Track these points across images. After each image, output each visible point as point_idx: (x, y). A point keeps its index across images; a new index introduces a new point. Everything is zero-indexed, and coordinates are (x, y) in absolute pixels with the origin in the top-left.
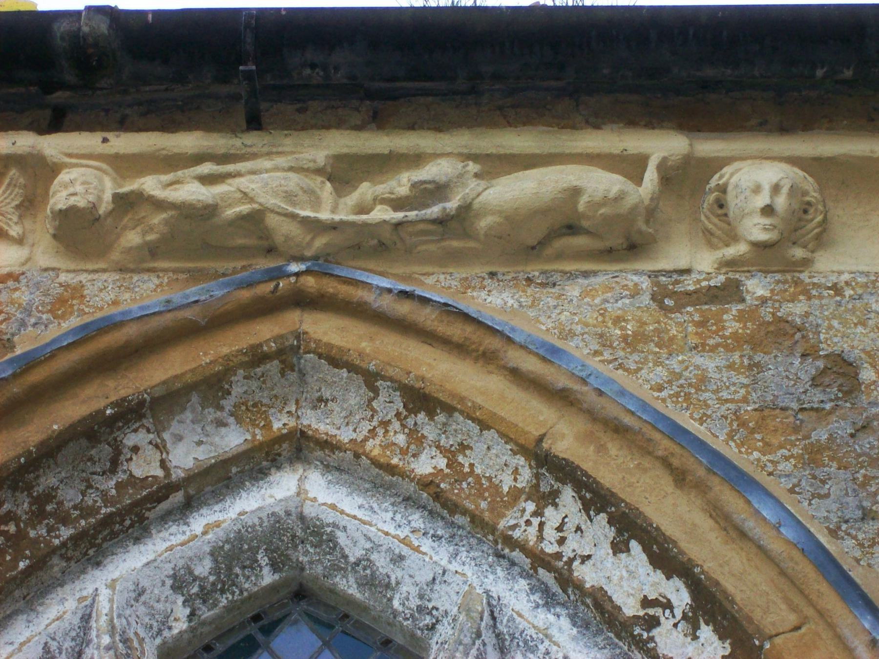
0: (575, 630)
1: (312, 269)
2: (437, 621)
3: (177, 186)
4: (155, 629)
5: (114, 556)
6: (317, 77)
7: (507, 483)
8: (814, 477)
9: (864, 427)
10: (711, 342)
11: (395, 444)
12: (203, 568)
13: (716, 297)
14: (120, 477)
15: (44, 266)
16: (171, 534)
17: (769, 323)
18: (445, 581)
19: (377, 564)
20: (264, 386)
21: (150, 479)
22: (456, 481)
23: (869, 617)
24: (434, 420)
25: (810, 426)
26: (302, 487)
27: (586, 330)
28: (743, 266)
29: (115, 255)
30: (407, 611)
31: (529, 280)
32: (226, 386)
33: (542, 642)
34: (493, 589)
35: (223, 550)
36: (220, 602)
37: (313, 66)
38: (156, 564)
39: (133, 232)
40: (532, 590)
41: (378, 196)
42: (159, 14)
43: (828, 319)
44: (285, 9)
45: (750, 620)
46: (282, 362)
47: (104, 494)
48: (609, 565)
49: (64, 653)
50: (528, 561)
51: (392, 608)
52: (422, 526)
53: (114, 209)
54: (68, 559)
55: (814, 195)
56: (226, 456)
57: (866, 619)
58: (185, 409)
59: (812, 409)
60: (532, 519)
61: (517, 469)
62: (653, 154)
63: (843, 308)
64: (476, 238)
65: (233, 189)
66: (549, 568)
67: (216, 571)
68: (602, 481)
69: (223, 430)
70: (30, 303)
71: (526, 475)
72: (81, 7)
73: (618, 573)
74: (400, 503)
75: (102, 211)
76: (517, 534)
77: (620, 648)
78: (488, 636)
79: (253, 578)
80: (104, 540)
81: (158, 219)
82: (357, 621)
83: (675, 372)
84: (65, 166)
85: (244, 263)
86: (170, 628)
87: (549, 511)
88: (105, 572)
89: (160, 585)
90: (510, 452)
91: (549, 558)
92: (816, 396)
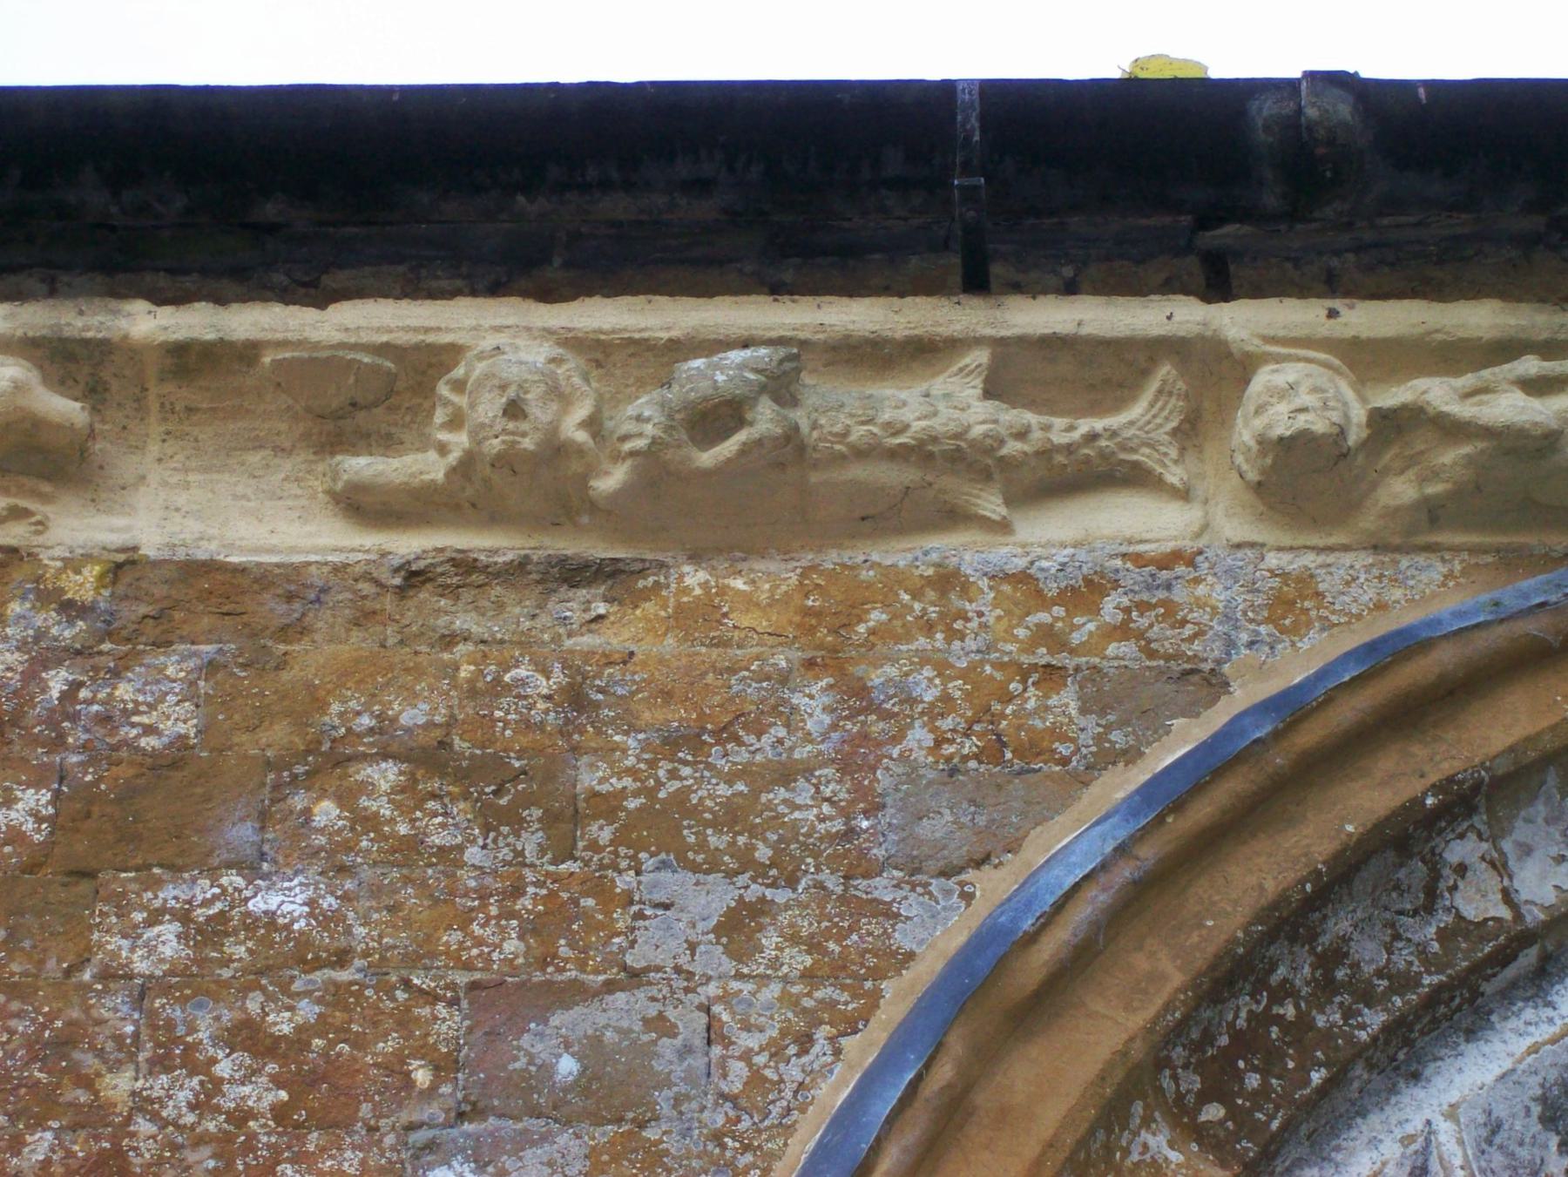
3: (1485, 397)
5: (1439, 1063)
14: (1440, 921)
15: (1236, 540)
16: (1528, 1024)
21: (1491, 923)
29: (1368, 521)
38: (1515, 1077)
39: (1402, 478)
42: (1437, 88)
47: (1421, 950)
53: (1369, 437)
58: (1536, 798)
81: (1451, 456)
84: (1266, 358)
88: (1433, 1091)
89: (1523, 1114)
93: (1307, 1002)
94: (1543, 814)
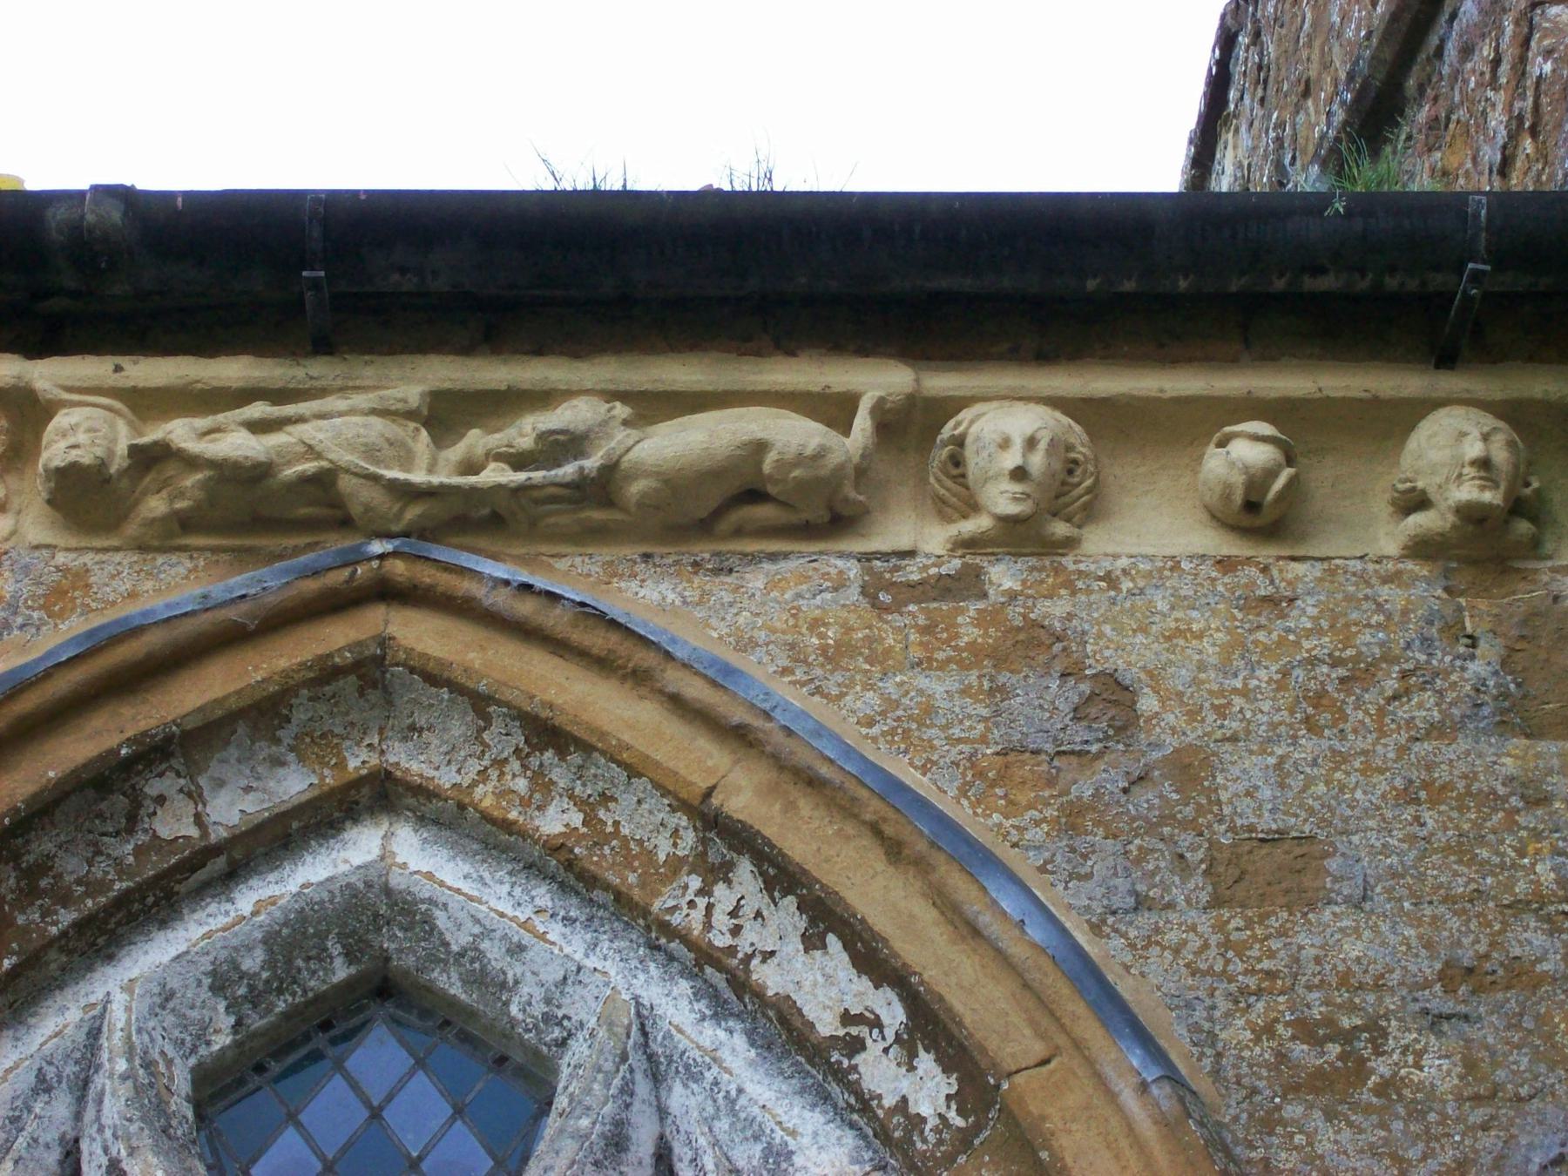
0: (753, 1053)
1: (402, 550)
2: (570, 1035)
4: (189, 1045)
5: (132, 947)
6: (409, 283)
7: (664, 849)
8: (1073, 850)
9: (1141, 778)
10: (940, 655)
11: (514, 792)
12: (252, 962)
13: (949, 590)
15: (35, 543)
16: (209, 915)
17: (1019, 629)
18: (580, 982)
19: (488, 955)
20: (335, 710)
22: (596, 844)
23: (1138, 1052)
24: (565, 761)
25: (1069, 777)
26: (388, 848)
27: (773, 638)
28: (986, 547)
29: (132, 529)
30: (528, 1020)
31: (696, 564)
32: (285, 712)
33: (710, 1069)
34: (644, 994)
35: (280, 936)
36: (277, 1006)
37: (403, 270)
38: (189, 957)
39: (157, 496)
40: (697, 995)
41: (492, 449)
42: (197, 200)
43: (1098, 624)
44: (366, 191)
45: (983, 1051)
46: (360, 677)
47: (118, 862)
48: (799, 966)
49: (65, 1080)
50: (692, 955)
51: (509, 1015)
52: (550, 904)
53: (129, 467)
54: (70, 952)
55: (1082, 450)
56: (283, 808)
57: (1134, 1053)
59: (1072, 752)
60: (696, 899)
61: (676, 831)
62: (865, 393)
63: (1118, 608)
64: (625, 510)
65: (293, 440)
66: (720, 967)
67: (270, 964)
68: (790, 853)
69: (281, 771)
70: (16, 596)
71: (689, 838)
72: (86, 187)
73: (811, 978)
74: (519, 871)
75: (113, 470)
76: (676, 919)
77: (813, 1077)
78: (636, 1059)
79: (321, 973)
80: (119, 924)
82: (461, 1031)
83: (890, 699)
85: (308, 540)
86: (208, 1043)
87: (720, 889)
88: (120, 969)
90: (668, 809)
91: (719, 954)
92: (1078, 735)
93: (10, 905)
94: (236, 755)
